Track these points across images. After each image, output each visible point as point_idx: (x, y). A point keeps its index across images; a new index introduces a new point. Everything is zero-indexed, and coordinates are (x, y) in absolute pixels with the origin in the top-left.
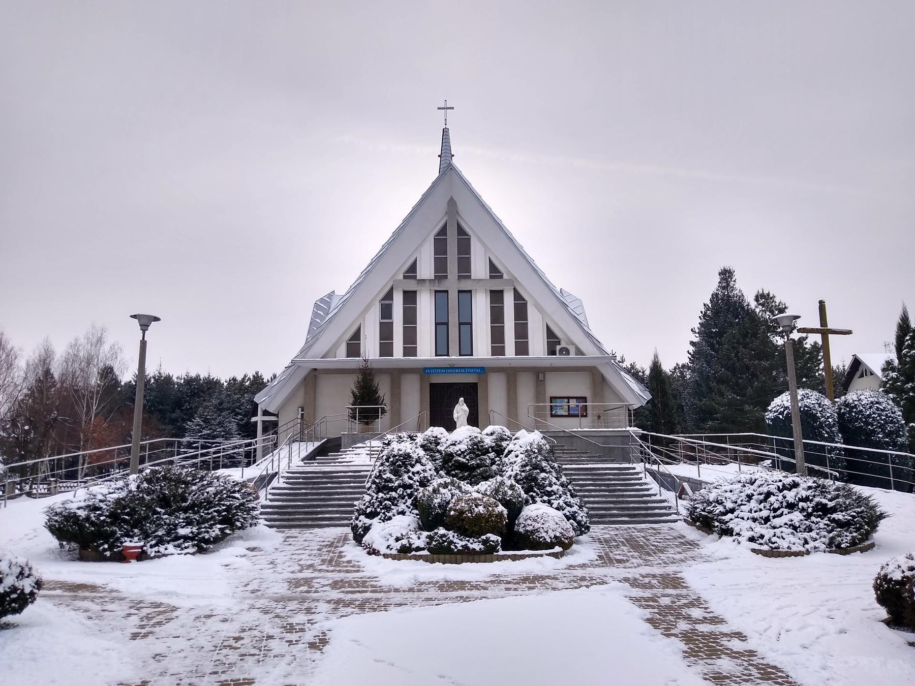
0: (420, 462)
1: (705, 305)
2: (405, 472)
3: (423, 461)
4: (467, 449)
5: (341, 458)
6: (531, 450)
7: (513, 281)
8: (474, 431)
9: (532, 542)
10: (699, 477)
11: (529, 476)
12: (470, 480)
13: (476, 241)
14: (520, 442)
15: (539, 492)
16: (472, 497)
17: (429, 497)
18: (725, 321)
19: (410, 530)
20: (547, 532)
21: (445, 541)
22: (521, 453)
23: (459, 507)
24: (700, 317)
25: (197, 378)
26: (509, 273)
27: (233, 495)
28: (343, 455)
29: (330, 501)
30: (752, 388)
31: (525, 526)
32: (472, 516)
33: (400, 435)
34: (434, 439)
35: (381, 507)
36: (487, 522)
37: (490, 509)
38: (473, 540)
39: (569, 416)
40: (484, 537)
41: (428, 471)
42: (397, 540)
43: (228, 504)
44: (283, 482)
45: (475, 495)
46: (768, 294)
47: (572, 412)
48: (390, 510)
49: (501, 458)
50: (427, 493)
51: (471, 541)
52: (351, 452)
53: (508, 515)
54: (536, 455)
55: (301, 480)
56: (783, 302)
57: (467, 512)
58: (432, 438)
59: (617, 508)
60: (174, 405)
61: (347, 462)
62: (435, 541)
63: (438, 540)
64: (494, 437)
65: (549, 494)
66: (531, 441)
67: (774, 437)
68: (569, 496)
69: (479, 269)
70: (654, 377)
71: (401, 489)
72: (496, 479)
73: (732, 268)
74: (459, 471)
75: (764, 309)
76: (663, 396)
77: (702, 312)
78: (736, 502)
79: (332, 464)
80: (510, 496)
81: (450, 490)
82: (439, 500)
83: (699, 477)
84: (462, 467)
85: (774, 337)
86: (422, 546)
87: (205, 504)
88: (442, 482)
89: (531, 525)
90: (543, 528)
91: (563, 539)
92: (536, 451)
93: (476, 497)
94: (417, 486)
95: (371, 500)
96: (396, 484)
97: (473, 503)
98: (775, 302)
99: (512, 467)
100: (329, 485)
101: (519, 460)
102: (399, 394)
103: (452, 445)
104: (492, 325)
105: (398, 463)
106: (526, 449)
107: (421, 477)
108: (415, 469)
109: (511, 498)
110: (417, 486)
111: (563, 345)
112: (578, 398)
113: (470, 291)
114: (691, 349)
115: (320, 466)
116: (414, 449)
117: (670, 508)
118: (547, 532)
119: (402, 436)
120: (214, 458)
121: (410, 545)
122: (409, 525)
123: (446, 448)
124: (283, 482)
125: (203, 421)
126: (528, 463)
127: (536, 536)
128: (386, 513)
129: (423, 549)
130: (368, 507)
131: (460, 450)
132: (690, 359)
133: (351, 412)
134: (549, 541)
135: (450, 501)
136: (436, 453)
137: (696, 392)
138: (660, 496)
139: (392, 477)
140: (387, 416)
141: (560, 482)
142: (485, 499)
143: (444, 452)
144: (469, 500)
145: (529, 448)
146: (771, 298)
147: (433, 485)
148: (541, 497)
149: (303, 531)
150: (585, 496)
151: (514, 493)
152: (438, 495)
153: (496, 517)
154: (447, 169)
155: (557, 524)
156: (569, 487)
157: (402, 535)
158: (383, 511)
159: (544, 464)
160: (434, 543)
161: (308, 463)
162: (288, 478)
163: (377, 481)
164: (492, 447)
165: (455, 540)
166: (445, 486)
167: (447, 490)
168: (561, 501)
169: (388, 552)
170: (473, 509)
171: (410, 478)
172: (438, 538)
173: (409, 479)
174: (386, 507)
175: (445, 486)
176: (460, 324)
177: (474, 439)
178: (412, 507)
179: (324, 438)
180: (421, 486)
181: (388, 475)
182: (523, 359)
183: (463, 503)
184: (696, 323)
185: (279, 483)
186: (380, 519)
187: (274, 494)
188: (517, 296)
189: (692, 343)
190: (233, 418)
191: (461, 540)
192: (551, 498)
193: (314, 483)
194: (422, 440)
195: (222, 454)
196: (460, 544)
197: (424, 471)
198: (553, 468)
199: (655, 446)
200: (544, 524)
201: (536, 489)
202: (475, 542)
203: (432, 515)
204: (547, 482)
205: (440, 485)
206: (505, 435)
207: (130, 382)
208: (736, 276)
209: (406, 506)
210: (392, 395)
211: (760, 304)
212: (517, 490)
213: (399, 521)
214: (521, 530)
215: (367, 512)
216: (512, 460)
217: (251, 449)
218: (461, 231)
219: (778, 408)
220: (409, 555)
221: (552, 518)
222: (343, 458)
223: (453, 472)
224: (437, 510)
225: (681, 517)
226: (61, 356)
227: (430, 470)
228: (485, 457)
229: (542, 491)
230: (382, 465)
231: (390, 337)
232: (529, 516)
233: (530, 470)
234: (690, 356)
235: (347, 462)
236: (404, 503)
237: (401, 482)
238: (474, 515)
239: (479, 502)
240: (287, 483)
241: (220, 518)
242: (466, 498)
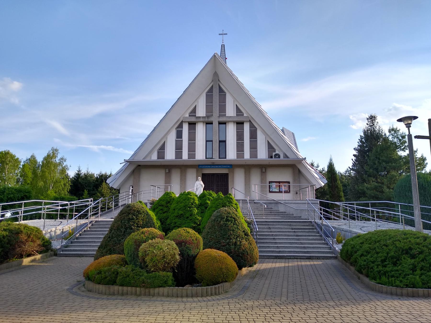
56: (404, 132)
69: (230, 112)
77: (359, 140)
120: (47, 211)
184: (356, 145)
189: (354, 155)
199: (327, 209)
210: (181, 179)
217: (73, 207)
218: (221, 90)
234: (353, 163)
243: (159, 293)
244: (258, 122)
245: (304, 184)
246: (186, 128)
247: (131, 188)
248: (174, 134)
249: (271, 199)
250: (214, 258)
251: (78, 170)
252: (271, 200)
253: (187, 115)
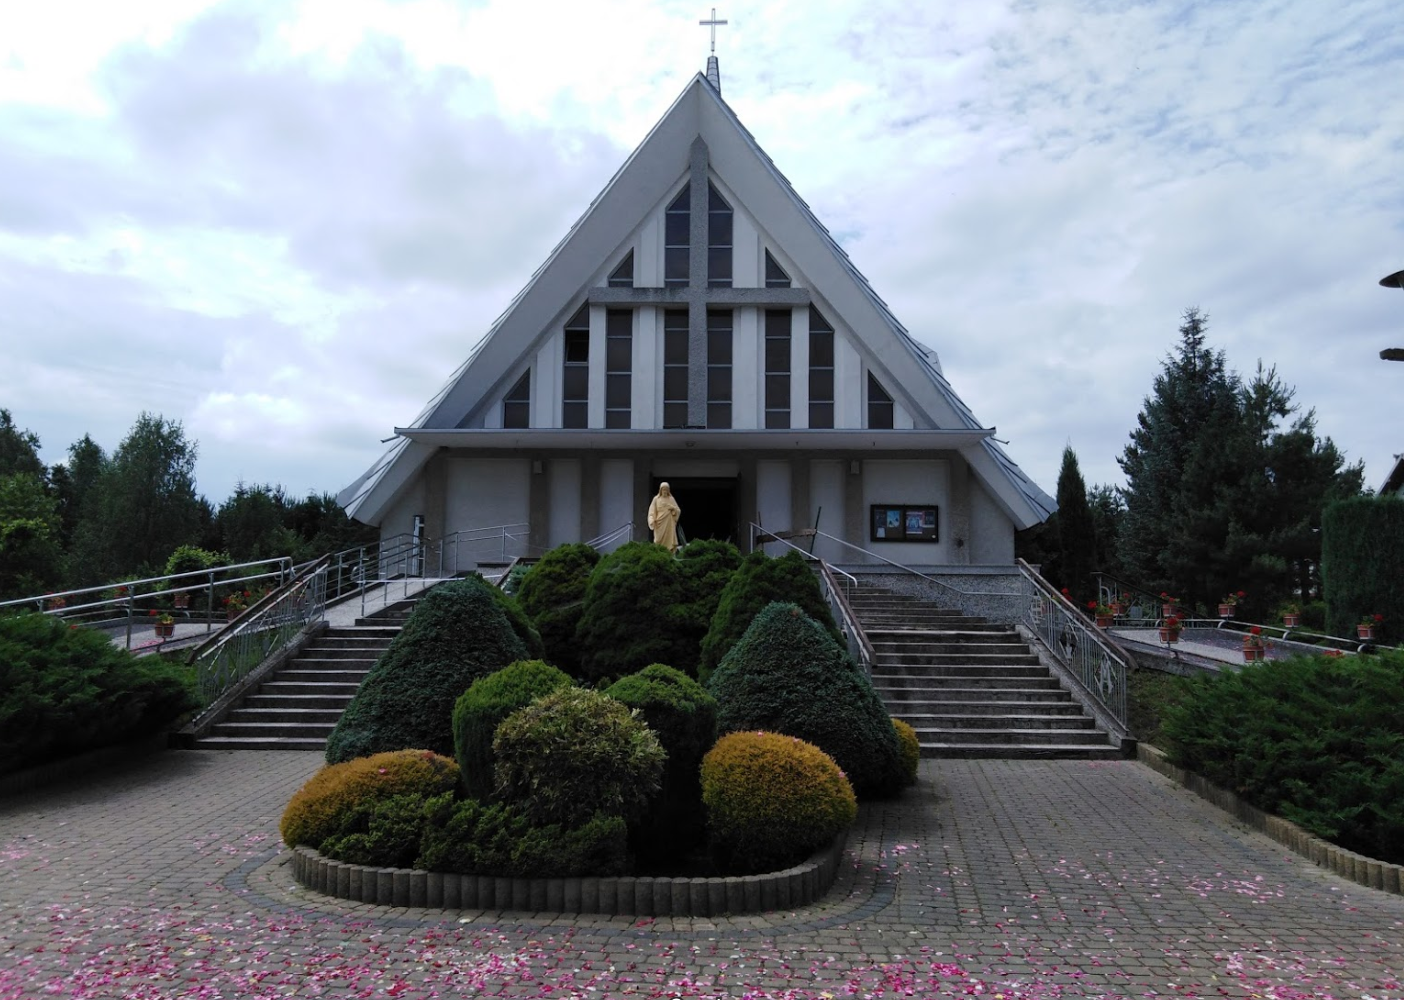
26: (803, 277)
69: (747, 272)
188: (817, 322)
218: (716, 200)
243: (579, 901)
244: (841, 305)
246: (598, 329)
247: (417, 522)
248: (556, 346)
249: (882, 563)
250: (795, 771)
252: (883, 565)
253: (603, 283)
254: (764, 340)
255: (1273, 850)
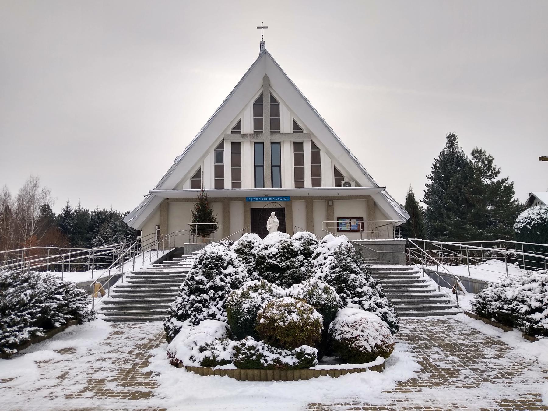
0: (232, 265)
1: (435, 160)
2: (217, 274)
3: (236, 263)
4: (278, 252)
5: (182, 262)
6: (341, 253)
7: (310, 135)
8: (285, 236)
9: (349, 351)
10: (469, 275)
11: (339, 277)
12: (281, 281)
13: (284, 106)
14: (327, 245)
15: (350, 294)
16: (284, 302)
17: (238, 302)
18: (452, 169)
19: (216, 339)
20: (367, 340)
21: (254, 354)
22: (329, 256)
23: (270, 314)
24: (432, 168)
25: (104, 212)
26: (307, 129)
27: (56, 296)
28: (183, 259)
29: (141, 304)
30: (471, 213)
31: (342, 333)
32: (284, 325)
33: (222, 242)
34: (248, 243)
35: (192, 309)
36: (302, 331)
37: (305, 316)
38: (286, 353)
39: (351, 231)
40: (298, 349)
41: (240, 273)
42: (202, 350)
43: (44, 306)
44: (127, 282)
45: (288, 300)
46: (481, 150)
47: (352, 228)
48: (200, 313)
49: (308, 260)
50: (235, 297)
51: (284, 354)
52: (190, 257)
53: (323, 322)
54: (345, 257)
55: (142, 280)
56: (491, 155)
57: (279, 321)
58: (246, 243)
59: (404, 302)
60: (88, 229)
61: (186, 265)
62: (243, 354)
63: (246, 353)
64: (302, 241)
65: (360, 295)
66: (340, 243)
67: (522, 243)
68: (379, 298)
69: (286, 126)
70: (409, 204)
71: (212, 291)
72: (309, 282)
73: (456, 134)
74: (271, 273)
75: (477, 160)
76: (415, 217)
77: (433, 164)
78: (542, 302)
79: (175, 266)
80: (325, 300)
81: (261, 294)
82: (248, 305)
83: (469, 275)
84: (273, 268)
85: (484, 179)
86: (228, 358)
87: (18, 306)
88: (252, 286)
89: (349, 332)
90: (362, 336)
91: (384, 348)
92: (346, 253)
93: (288, 302)
94: (228, 288)
95: (182, 302)
96: (208, 286)
97: (285, 310)
98: (486, 156)
99: (321, 269)
100: (165, 284)
101: (328, 261)
102: (229, 216)
103: (264, 248)
104: (295, 167)
105: (210, 266)
106: (335, 251)
107: (232, 279)
108: (227, 272)
109: (326, 302)
110: (228, 288)
111: (346, 180)
112: (357, 218)
113: (279, 143)
114: (426, 189)
115: (165, 268)
116: (226, 251)
117: (449, 301)
118: (367, 340)
119: (224, 243)
121: (215, 357)
122: (216, 332)
123: (259, 252)
124: (127, 282)
125: (103, 238)
126: (338, 265)
127: (355, 345)
128: (197, 315)
129: (229, 362)
130: (180, 309)
131: (272, 253)
132: (425, 196)
133: (192, 228)
134: (370, 351)
135: (260, 306)
136: (249, 256)
137: (431, 217)
138: (439, 291)
139: (204, 279)
140: (219, 231)
141: (369, 282)
142: (299, 305)
143: (257, 255)
144: (280, 306)
145: (338, 250)
146: (483, 153)
147: (243, 288)
148: (352, 298)
149: (134, 324)
150: (393, 297)
151: (329, 296)
152: (247, 299)
153: (311, 325)
154: (264, 53)
155: (377, 330)
156: (377, 287)
157: (207, 345)
158: (194, 313)
159: (353, 265)
160: (241, 356)
161: (157, 266)
162: (132, 278)
163: (190, 283)
164: (301, 251)
165: (266, 353)
166: (255, 289)
167: (257, 294)
168: (371, 302)
169: (191, 364)
170: (286, 317)
171: (222, 280)
172: (246, 350)
173: (220, 280)
174: (197, 309)
175: (255, 289)
176: (272, 166)
177: (285, 243)
178: (222, 309)
179: (173, 248)
180: (232, 288)
181: (200, 277)
182: (319, 190)
183: (274, 310)
185: (122, 282)
186: (191, 322)
187: (117, 292)
188: (313, 146)
189: (427, 185)
190: (126, 237)
191: (272, 353)
192: (362, 299)
193: (153, 282)
194: (238, 244)
195: (70, 259)
196: (271, 357)
197: (236, 273)
198: (361, 269)
200: (363, 331)
201: (346, 290)
202: (288, 355)
203: (241, 321)
204: (357, 283)
205: (250, 288)
206: (312, 240)
207: (62, 214)
208: (459, 139)
209: (217, 308)
211: (475, 157)
212: (331, 294)
213: (206, 327)
214: (338, 337)
215: (179, 314)
216: (320, 262)
218: (273, 99)
219: (526, 220)
220: (213, 369)
221: (372, 324)
222: (184, 262)
223: (265, 273)
224: (245, 316)
225: (461, 310)
226: (15, 198)
227: (242, 272)
228: (294, 259)
229: (353, 292)
230: (195, 267)
231: (222, 175)
232: (346, 321)
233: (340, 271)
234: (425, 194)
235: (186, 265)
236: (215, 305)
237: (212, 284)
238: (286, 324)
239: (292, 308)
240: (130, 282)
241: (34, 320)
242: (278, 303)
244: (323, 142)
245: (381, 221)
251: (67, 206)
254: (253, 119)
255: (216, 332)
